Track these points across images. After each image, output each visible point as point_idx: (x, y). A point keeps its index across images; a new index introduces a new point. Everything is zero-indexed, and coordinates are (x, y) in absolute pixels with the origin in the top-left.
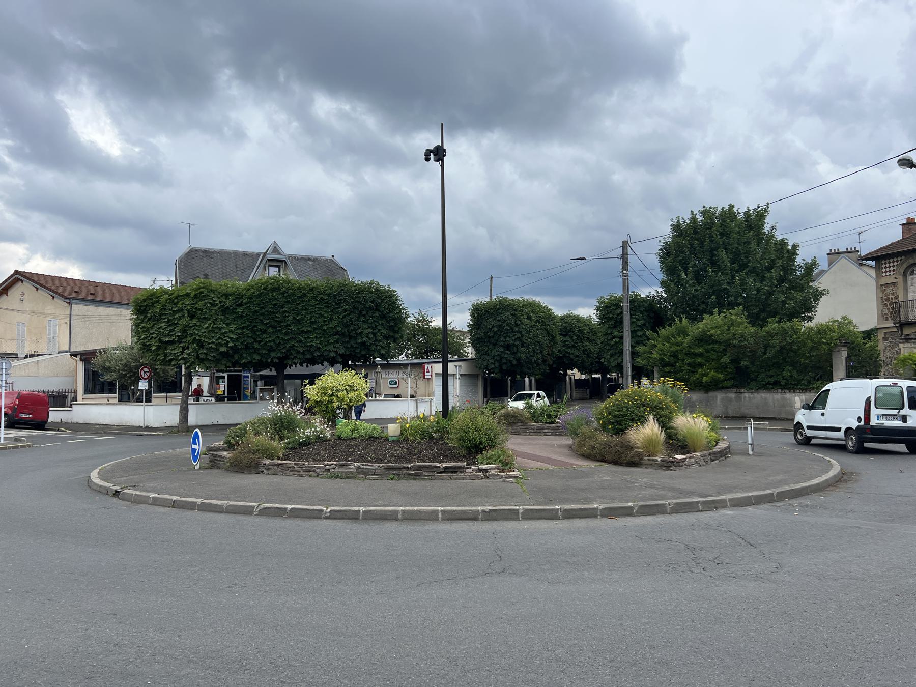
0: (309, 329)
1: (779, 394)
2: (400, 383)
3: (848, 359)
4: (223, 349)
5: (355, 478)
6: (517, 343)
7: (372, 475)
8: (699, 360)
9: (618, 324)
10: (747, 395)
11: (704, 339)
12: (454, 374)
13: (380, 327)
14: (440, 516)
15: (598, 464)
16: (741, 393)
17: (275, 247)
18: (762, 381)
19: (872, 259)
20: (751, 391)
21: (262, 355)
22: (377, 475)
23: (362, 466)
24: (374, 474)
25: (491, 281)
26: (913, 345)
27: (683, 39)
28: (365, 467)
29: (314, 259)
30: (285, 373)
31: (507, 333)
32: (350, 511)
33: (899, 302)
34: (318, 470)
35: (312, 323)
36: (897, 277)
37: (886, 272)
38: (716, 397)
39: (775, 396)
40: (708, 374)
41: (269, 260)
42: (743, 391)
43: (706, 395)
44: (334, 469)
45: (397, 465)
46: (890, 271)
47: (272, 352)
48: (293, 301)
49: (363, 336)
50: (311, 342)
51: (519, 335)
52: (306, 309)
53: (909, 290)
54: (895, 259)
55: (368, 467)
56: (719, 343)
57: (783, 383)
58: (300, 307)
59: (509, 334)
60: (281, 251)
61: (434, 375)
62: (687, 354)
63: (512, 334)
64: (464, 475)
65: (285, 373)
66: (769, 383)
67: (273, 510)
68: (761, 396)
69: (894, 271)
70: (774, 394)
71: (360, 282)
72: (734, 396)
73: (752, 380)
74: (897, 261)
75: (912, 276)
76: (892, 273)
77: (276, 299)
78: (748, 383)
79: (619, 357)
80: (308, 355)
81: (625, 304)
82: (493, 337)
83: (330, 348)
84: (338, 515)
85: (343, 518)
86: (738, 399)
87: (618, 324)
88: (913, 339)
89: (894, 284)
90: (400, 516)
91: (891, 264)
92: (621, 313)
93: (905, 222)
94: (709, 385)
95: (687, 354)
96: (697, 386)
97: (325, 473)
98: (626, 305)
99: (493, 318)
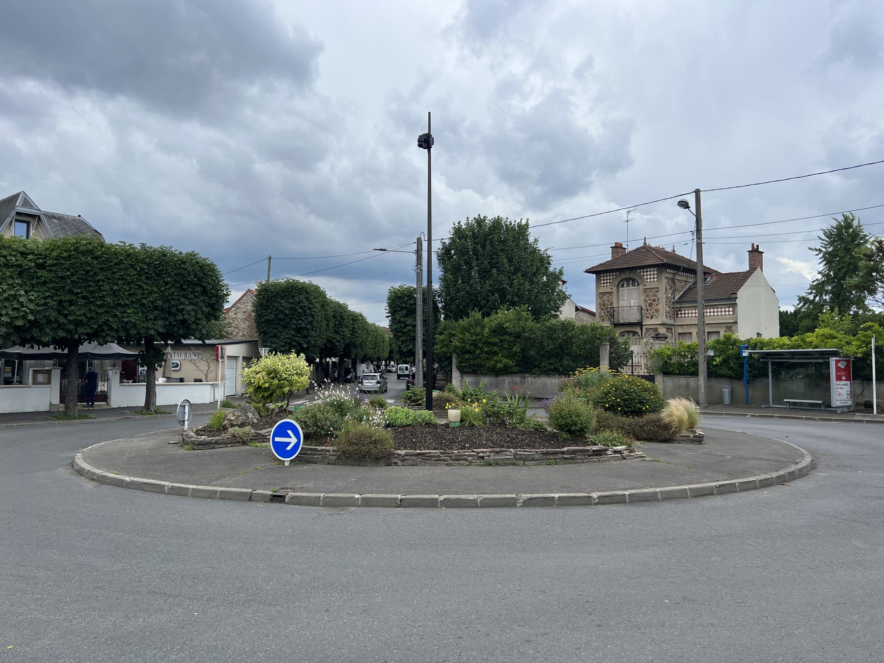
0: (127, 302)
1: (557, 378)
2: (182, 365)
3: (611, 353)
4: (20, 323)
5: (514, 464)
6: (309, 326)
7: (531, 461)
8: (496, 349)
9: (409, 313)
10: (530, 379)
11: (500, 330)
12: (236, 357)
13: (201, 304)
14: (689, 494)
15: (168, 452)
16: (525, 377)
17: (25, 199)
18: (544, 368)
19: (593, 272)
20: (533, 376)
21: (68, 331)
22: (535, 460)
23: (519, 453)
24: (533, 460)
25: (270, 261)
26: (661, 342)
27: (318, 48)
28: (522, 453)
29: (59, 217)
30: (79, 352)
31: (299, 317)
32: (616, 496)
33: (613, 308)
34: (470, 458)
35: (130, 295)
36: (612, 288)
37: (604, 283)
38: (504, 381)
39: (553, 380)
40: (501, 361)
41: (18, 214)
42: (527, 375)
43: (496, 379)
44: (488, 456)
45: (548, 450)
46: (607, 283)
47: (79, 328)
48: (109, 269)
49: (184, 313)
50: (128, 317)
51: (310, 319)
52: (123, 279)
53: (620, 298)
54: (611, 274)
55: (526, 453)
56: (510, 334)
57: (561, 369)
58: (117, 276)
59: (302, 318)
60: (34, 206)
61: (226, 358)
62: (484, 343)
63: (305, 317)
64: (608, 457)
65: (79, 352)
66: (550, 370)
67: (539, 500)
68: (542, 380)
69: (610, 283)
70: (552, 378)
71: (177, 252)
72: (519, 380)
73: (535, 366)
74: (613, 275)
75: (623, 288)
76: (608, 284)
77: (90, 264)
78: (531, 369)
79: (410, 343)
80: (122, 333)
81: (418, 296)
82: (284, 319)
83: (150, 324)
84: (607, 500)
85: (612, 503)
86: (523, 383)
87: (409, 313)
88: (662, 337)
89: (610, 293)
90: (659, 497)
91: (608, 278)
92: (415, 304)
93: (614, 245)
94: (499, 370)
95: (484, 343)
96: (490, 371)
97: (478, 461)
98: (419, 297)
99: (285, 300)
